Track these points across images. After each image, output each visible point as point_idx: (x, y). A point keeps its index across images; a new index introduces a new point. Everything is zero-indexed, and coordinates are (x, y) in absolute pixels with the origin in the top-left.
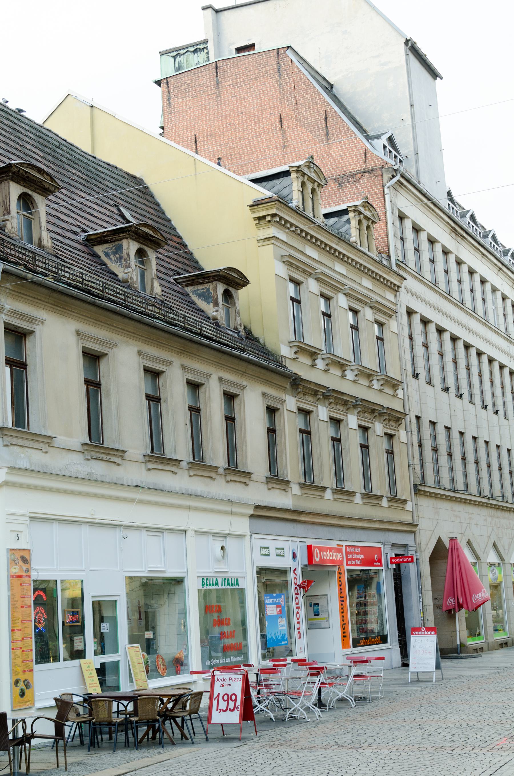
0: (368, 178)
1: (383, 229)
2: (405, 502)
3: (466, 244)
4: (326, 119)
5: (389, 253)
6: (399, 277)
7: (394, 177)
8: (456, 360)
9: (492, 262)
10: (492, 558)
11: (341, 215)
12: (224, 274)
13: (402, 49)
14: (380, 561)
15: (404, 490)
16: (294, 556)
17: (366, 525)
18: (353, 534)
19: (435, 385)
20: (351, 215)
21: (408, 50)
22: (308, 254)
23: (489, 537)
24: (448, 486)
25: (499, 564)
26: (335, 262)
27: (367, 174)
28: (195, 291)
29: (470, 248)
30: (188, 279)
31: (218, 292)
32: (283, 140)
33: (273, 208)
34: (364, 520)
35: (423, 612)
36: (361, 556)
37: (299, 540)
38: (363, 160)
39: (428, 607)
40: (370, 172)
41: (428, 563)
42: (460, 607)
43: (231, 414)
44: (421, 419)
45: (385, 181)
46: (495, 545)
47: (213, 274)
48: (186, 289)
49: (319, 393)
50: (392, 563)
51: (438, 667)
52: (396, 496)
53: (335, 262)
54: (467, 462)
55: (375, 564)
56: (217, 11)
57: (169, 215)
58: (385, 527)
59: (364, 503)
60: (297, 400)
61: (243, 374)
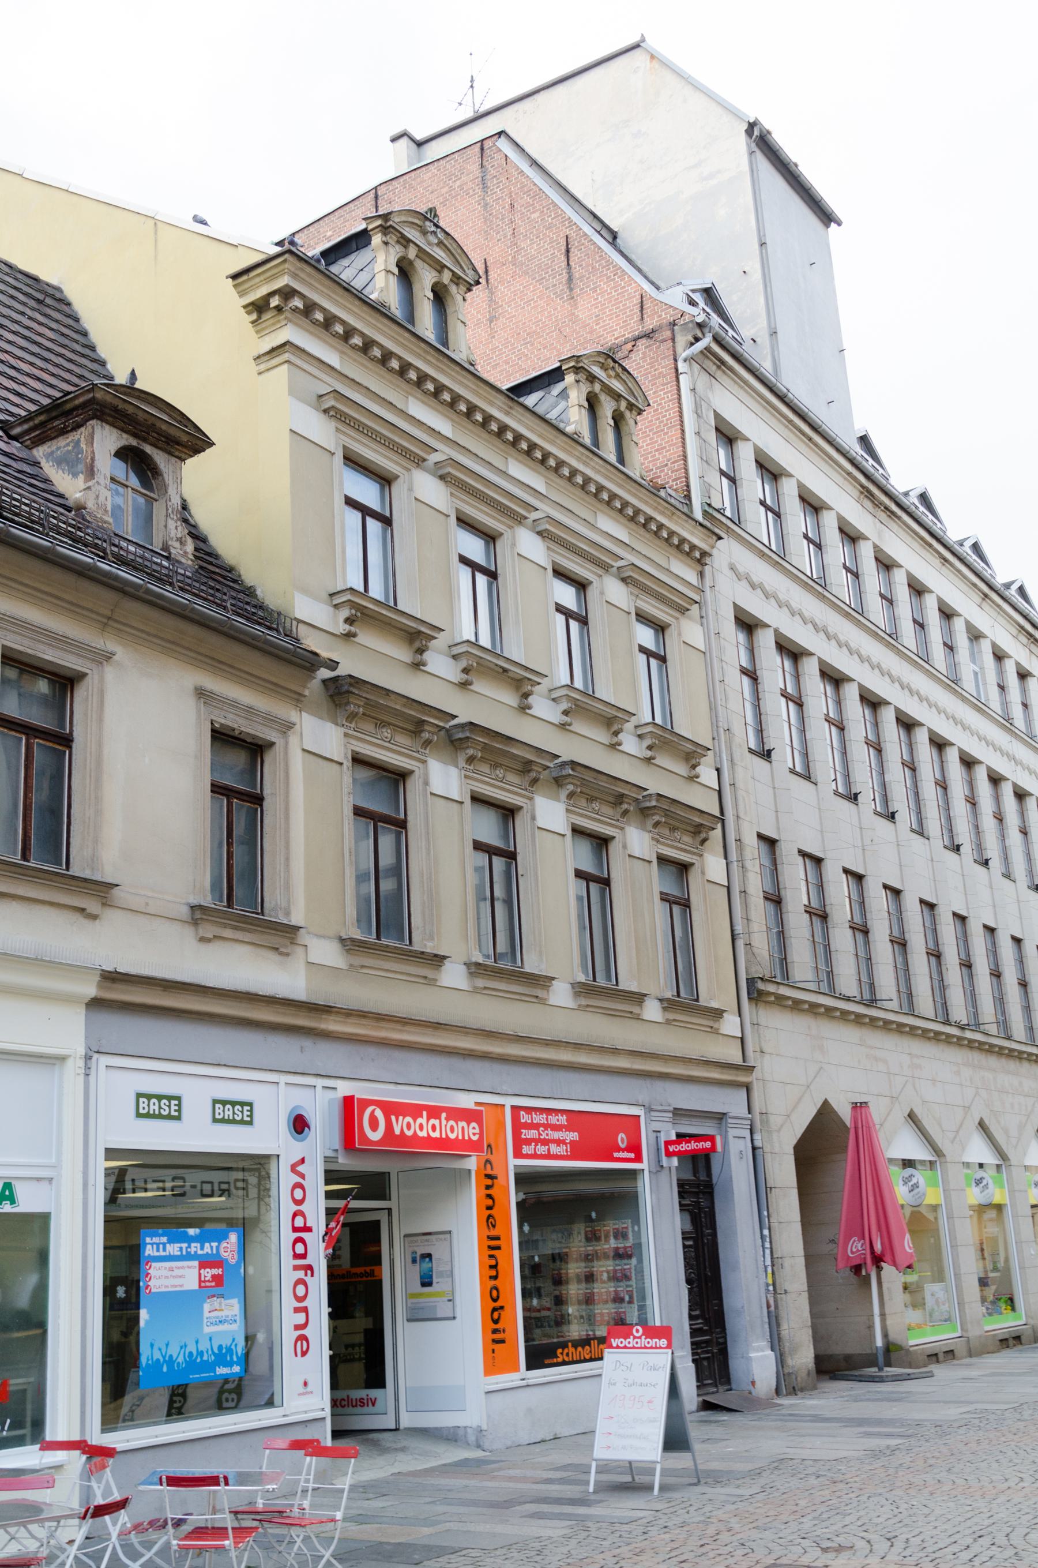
0: (646, 347)
1: (674, 444)
2: (718, 1014)
3: (900, 530)
4: (568, 251)
5: (689, 491)
6: (700, 528)
7: (697, 339)
8: (879, 744)
9: (965, 577)
10: (979, 1151)
11: (549, 385)
12: (109, 398)
13: (741, 143)
14: (635, 1148)
15: (716, 986)
16: (300, 1125)
17: (583, 1058)
18: (545, 1080)
19: (819, 780)
20: (570, 378)
21: (753, 145)
22: (411, 412)
23: (967, 1108)
24: (852, 991)
25: (998, 1166)
26: (510, 459)
27: (644, 340)
28: (52, 453)
29: (910, 539)
30: (31, 424)
31: (95, 445)
32: (490, 306)
33: (282, 274)
34: (577, 1046)
35: (773, 1273)
36: (572, 1136)
37: (320, 1082)
38: (637, 317)
39: (787, 1263)
40: (648, 335)
41: (791, 1159)
42: (878, 1260)
43: (63, 728)
44: (778, 844)
45: (679, 348)
46: (982, 1125)
47: (81, 400)
48: (35, 451)
49: (427, 727)
50: (669, 1154)
51: (675, 1440)
52: (697, 1000)
53: (510, 459)
54: (908, 951)
55: (616, 1155)
56: (420, 144)
57: (102, 352)
58: (648, 1069)
59: (581, 1008)
60: (346, 735)
61: (107, 623)
